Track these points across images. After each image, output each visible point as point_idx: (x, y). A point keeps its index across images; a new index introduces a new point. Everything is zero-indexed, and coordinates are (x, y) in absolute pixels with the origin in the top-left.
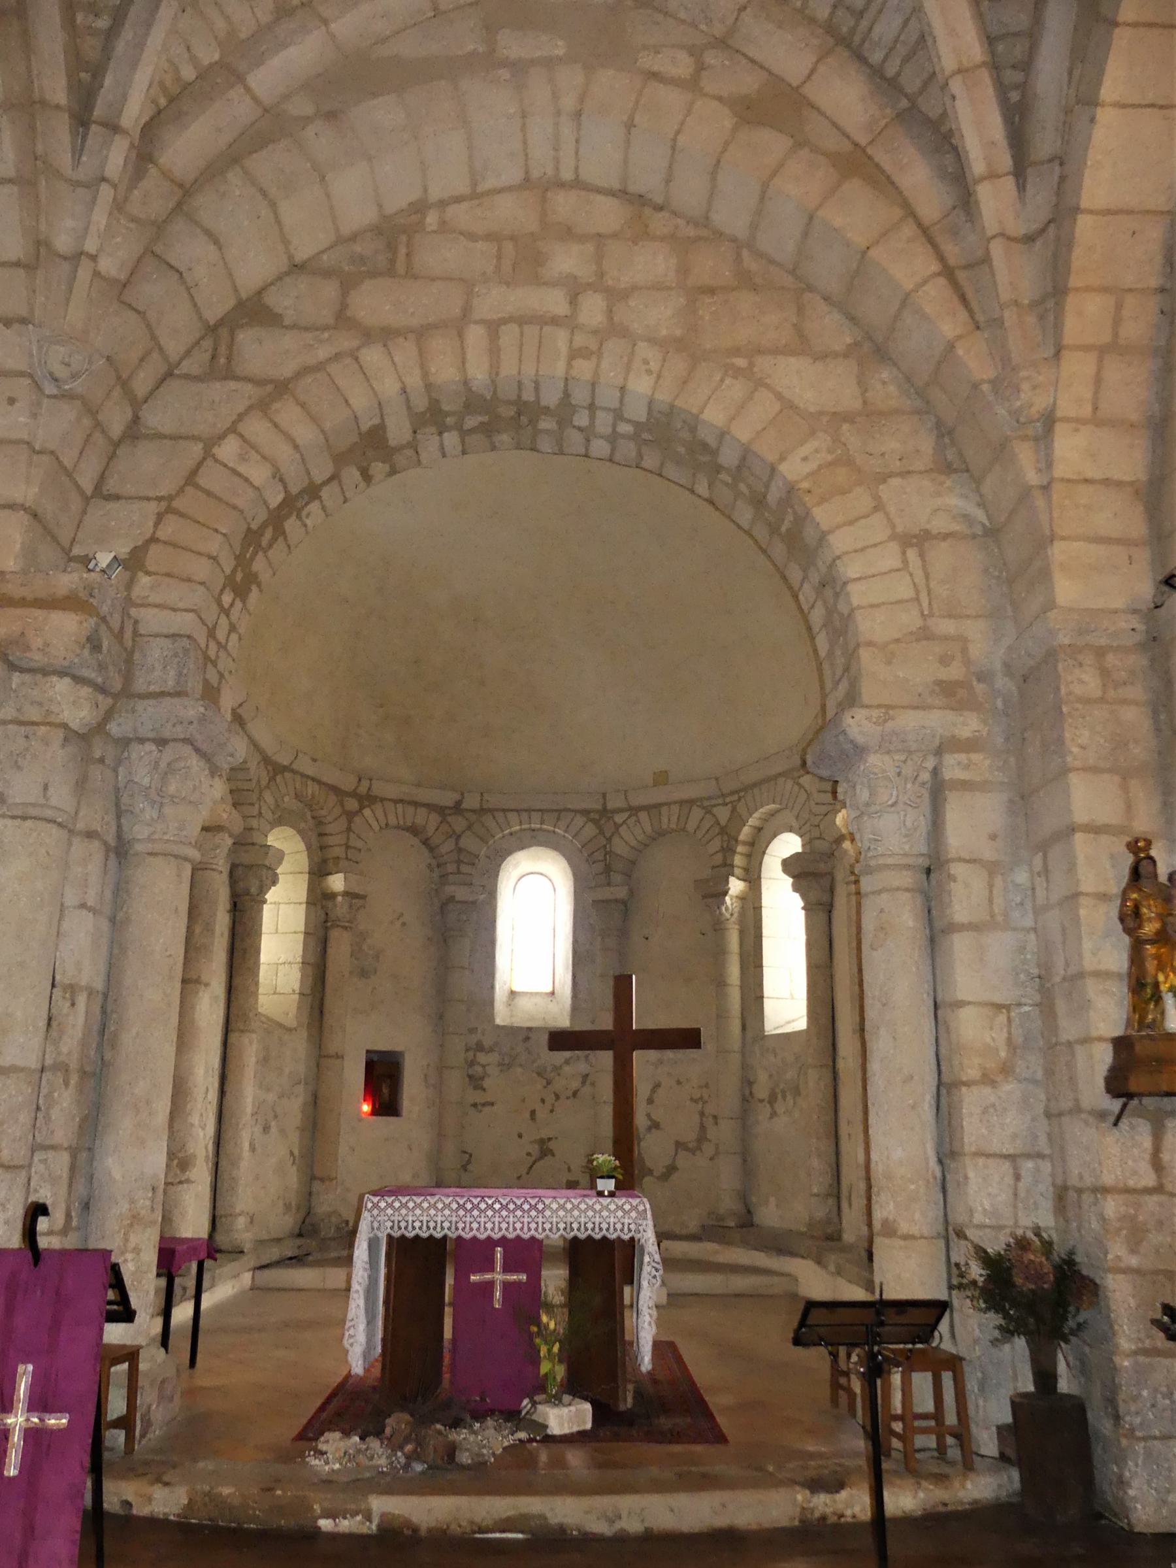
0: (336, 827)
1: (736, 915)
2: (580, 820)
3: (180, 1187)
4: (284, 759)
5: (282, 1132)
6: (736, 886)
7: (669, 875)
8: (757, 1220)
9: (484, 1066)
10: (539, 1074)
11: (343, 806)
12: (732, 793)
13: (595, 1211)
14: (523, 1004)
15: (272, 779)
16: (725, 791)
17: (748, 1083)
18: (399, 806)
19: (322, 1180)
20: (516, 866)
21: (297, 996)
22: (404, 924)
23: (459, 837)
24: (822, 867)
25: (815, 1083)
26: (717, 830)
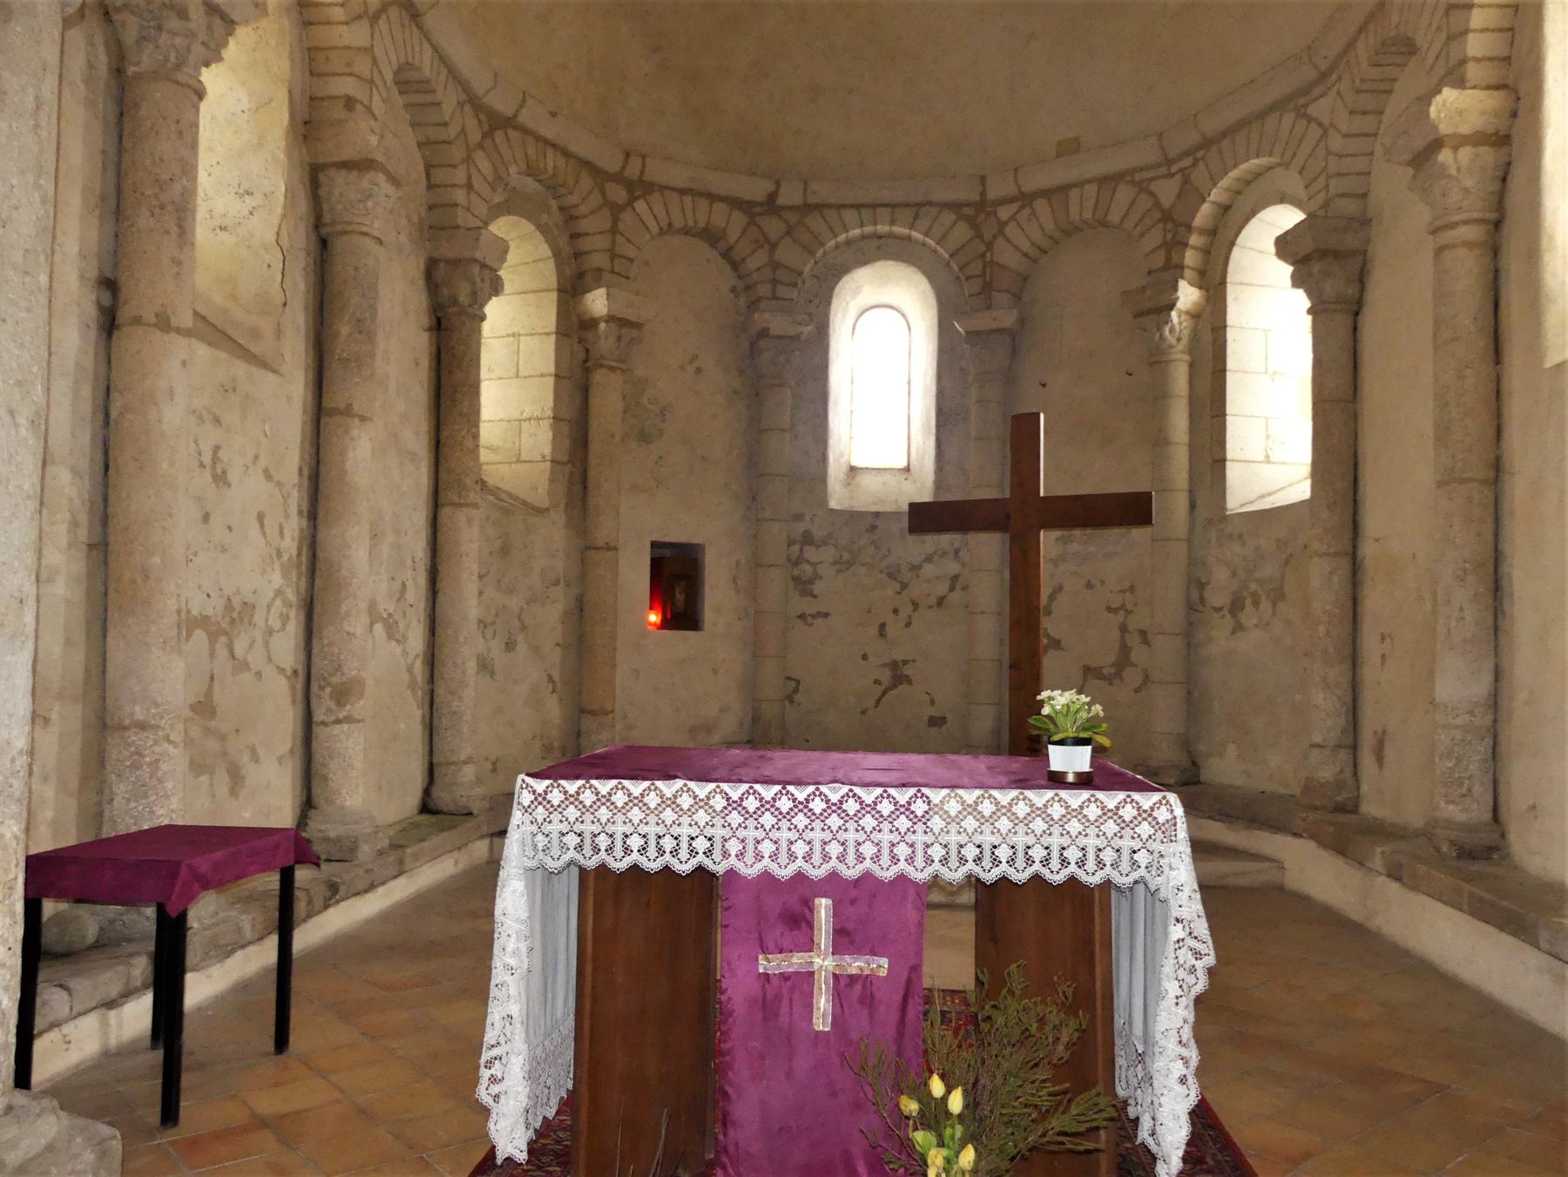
0: (594, 224)
1: (1184, 341)
2: (948, 217)
3: (337, 729)
4: (503, 104)
5: (535, 649)
6: (1188, 295)
7: (1083, 286)
8: (1203, 778)
9: (814, 565)
10: (891, 575)
11: (603, 193)
12: (1186, 154)
13: (1049, 819)
14: (868, 483)
15: (488, 134)
16: (1172, 154)
17: (1197, 584)
18: (688, 199)
19: (593, 713)
20: (857, 291)
21: (548, 464)
22: (699, 371)
23: (774, 246)
24: (1351, 241)
25: (1321, 578)
26: (1158, 215)
